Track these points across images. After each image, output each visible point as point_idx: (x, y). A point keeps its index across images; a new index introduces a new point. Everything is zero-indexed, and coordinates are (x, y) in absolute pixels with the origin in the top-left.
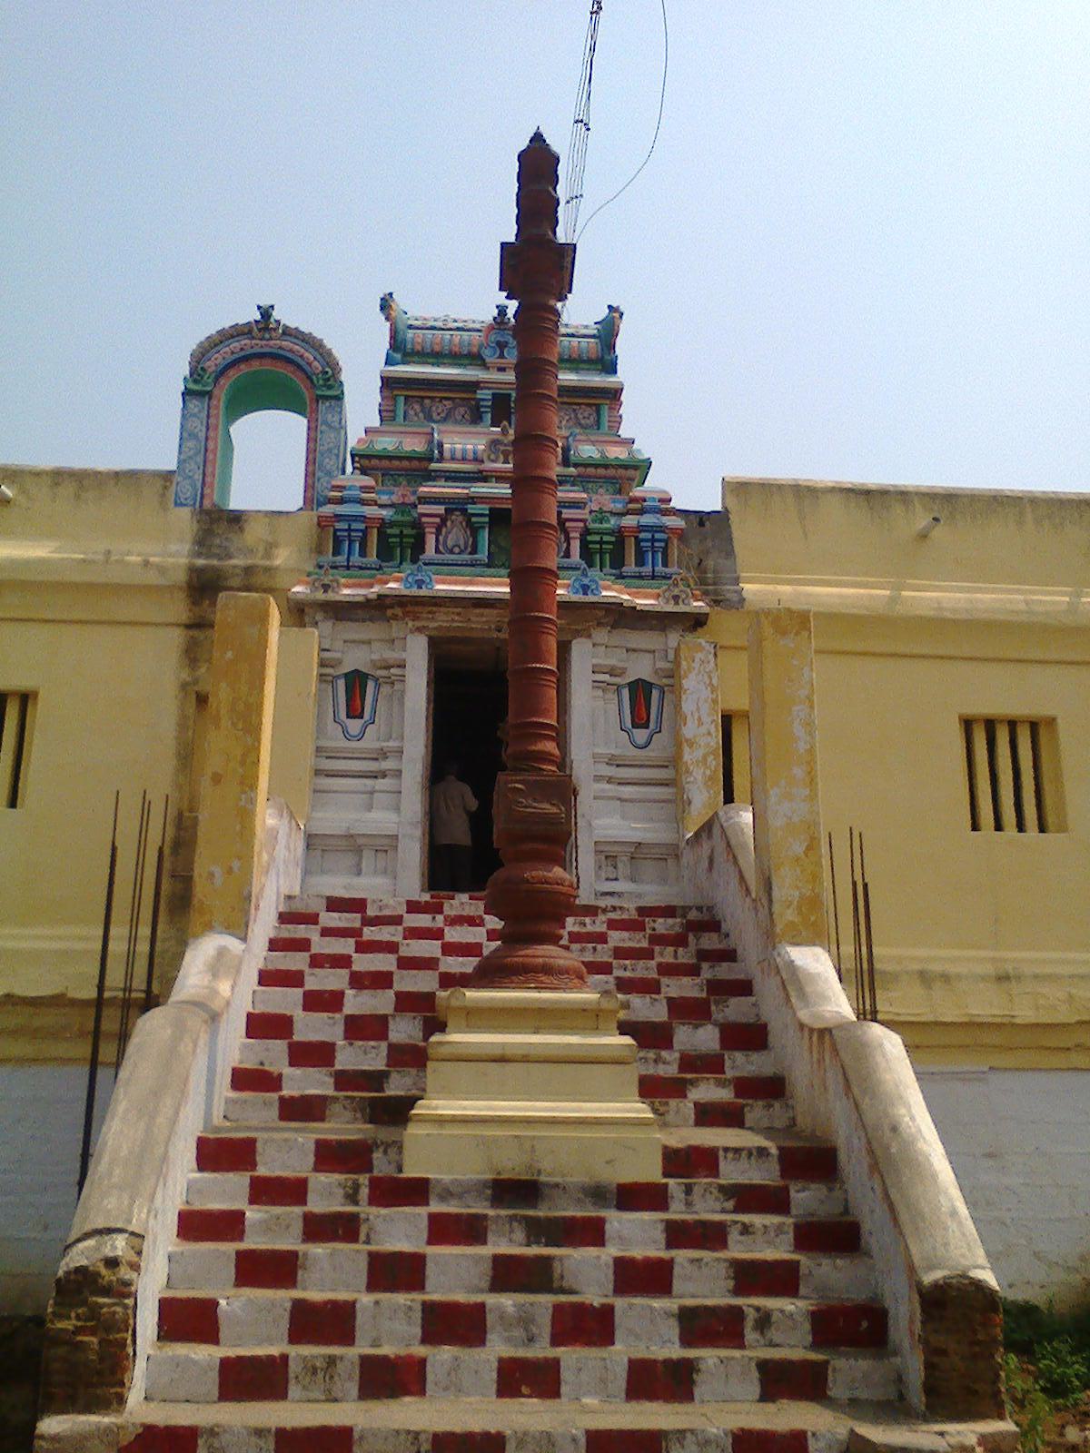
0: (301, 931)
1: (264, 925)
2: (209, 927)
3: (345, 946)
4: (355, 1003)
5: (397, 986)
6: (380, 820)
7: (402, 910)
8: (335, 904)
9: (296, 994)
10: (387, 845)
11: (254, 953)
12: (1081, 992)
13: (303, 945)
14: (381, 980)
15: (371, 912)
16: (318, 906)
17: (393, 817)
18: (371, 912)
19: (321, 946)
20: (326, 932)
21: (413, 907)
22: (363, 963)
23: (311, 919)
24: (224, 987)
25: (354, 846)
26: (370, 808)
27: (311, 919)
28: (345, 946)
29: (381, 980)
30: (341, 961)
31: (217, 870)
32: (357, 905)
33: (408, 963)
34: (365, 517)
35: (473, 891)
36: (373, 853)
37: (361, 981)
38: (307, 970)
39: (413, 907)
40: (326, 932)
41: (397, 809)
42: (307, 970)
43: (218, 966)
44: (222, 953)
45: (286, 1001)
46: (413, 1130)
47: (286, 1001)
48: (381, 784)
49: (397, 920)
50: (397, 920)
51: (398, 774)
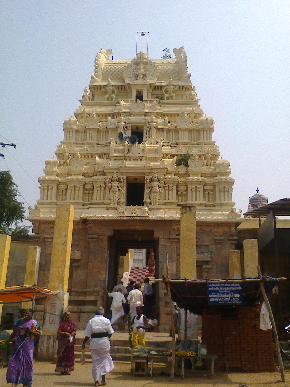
0: (133, 271)
1: (130, 270)
2: (125, 271)
3: (137, 272)
4: (138, 278)
5: (141, 276)
6: (141, 258)
7: (142, 269)
8: (136, 268)
9: (133, 277)
10: (142, 260)
11: (129, 273)
12: (284, 221)
13: (133, 272)
14: (140, 276)
15: (140, 269)
16: (134, 268)
17: (142, 257)
18: (140, 269)
19: (135, 272)
20: (135, 271)
21: (144, 268)
22: (139, 274)
23: (134, 269)
24: (127, 277)
25: (138, 260)
26: (140, 256)
27: (134, 269)
28: (137, 272)
29: (140, 276)
30: (137, 274)
31: (126, 266)
32: (138, 268)
33: (142, 274)
34: (119, 63)
35: (124, 99)
36: (97, 95)
37: (138, 276)
38: (136, 281)
39: (144, 268)
40: (135, 271)
41: (143, 256)
42: (136, 281)
43: (126, 275)
44: (126, 274)
45: (132, 277)
46: (141, 288)
47: (132, 277)
48: (141, 253)
49: (142, 270)
50: (142, 270)
51: (143, 252)
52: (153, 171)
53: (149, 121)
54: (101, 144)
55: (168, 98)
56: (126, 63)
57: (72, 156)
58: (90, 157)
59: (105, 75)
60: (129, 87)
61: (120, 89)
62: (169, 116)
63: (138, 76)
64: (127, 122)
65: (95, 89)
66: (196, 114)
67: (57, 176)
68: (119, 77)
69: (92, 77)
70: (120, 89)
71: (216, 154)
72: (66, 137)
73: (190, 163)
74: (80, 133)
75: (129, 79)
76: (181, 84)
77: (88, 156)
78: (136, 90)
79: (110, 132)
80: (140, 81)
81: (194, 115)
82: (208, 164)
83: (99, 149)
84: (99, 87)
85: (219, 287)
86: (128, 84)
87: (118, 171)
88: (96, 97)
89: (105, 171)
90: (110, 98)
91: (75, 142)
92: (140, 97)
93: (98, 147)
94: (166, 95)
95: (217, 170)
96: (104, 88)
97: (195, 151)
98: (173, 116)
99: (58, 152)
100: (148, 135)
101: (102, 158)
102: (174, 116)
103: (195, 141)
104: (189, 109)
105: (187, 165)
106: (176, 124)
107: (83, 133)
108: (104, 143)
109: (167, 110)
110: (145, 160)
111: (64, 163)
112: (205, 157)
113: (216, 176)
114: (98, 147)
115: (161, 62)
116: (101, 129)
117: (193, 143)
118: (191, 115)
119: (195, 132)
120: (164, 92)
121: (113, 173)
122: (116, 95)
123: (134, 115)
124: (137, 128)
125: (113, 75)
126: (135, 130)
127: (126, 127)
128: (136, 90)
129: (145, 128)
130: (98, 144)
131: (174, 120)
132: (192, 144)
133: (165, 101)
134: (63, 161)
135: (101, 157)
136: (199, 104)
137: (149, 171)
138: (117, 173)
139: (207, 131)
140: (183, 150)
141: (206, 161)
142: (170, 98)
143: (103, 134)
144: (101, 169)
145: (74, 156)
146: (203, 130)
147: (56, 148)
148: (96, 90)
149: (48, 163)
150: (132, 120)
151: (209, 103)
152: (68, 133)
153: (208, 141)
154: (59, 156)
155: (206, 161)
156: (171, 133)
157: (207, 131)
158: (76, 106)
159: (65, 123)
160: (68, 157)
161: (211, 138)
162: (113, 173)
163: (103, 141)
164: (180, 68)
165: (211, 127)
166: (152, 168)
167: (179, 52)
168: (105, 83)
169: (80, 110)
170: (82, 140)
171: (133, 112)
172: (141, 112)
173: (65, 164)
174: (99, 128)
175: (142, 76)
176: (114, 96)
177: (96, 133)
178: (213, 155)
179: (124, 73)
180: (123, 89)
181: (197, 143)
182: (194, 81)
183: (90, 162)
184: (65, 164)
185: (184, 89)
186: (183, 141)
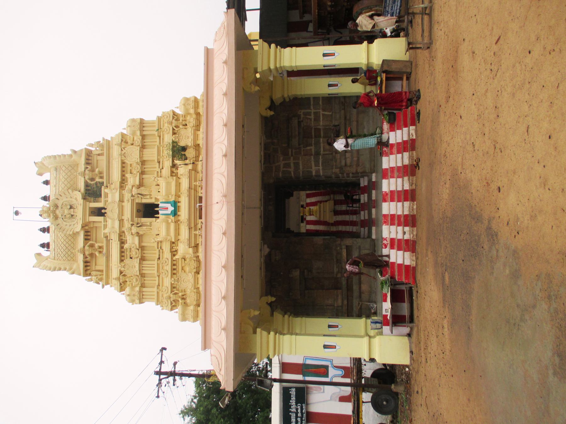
52: (193, 187)
53: (130, 195)
54: (159, 255)
55: (102, 178)
56: (54, 232)
57: (175, 289)
58: (175, 267)
59: (69, 258)
60: (86, 225)
61: (89, 237)
62: (124, 173)
63: (72, 216)
64: (132, 223)
65: (87, 270)
66: (122, 140)
67: (199, 305)
68: (72, 240)
69: (73, 273)
70: (89, 237)
71: (172, 114)
72: (151, 299)
73: (182, 144)
74: (145, 282)
75: (76, 225)
76: (83, 160)
77: (174, 269)
78: (89, 216)
79: (143, 244)
80: (79, 212)
81: (123, 143)
82: (184, 123)
83: (165, 256)
84: (86, 264)
85: (297, 413)
86: (83, 227)
87: (193, 229)
88: (98, 268)
89: (193, 245)
90: (100, 250)
91: (156, 287)
92: (99, 212)
93: (162, 286)
94: (98, 180)
95: (192, 111)
96: (87, 258)
97: (168, 138)
98: (124, 165)
99: (170, 307)
100: (148, 197)
101: (177, 253)
102: (123, 171)
103: (155, 166)
104: (116, 151)
105: (184, 149)
106: (135, 164)
107: (145, 278)
108: (157, 252)
109: (116, 176)
110: (179, 197)
111: (183, 299)
112: (175, 127)
113: (199, 145)
114: (162, 286)
115: (54, 188)
116: (140, 256)
117: (158, 143)
118: (123, 146)
119: (145, 167)
120: (92, 183)
121: (195, 235)
122: (96, 242)
123: (122, 215)
124: (138, 211)
125: (69, 248)
126: (142, 213)
127: (138, 223)
128: (89, 216)
129: (138, 200)
130: (159, 258)
131: (129, 166)
132: (160, 143)
133: (105, 180)
134: (180, 300)
135: (175, 253)
136: (110, 139)
137: (193, 191)
138: (195, 230)
139: (143, 127)
140: (167, 153)
141: (181, 127)
142: (101, 175)
143: (147, 254)
144: (191, 250)
145: (174, 288)
146: (141, 130)
147: (164, 310)
148: (89, 268)
149: (184, 318)
150: (129, 216)
151: (108, 125)
152: (144, 297)
153: (156, 125)
154: (174, 306)
155: (181, 127)
156: (145, 170)
157: (143, 127)
158: (111, 292)
159: (133, 301)
160: (176, 294)
161: (153, 122)
162: (195, 235)
163: (155, 254)
164: (61, 164)
165: (139, 121)
166: (190, 188)
167: (41, 168)
168: (81, 257)
169: (115, 284)
170: (153, 279)
171: (119, 216)
172: (119, 205)
173: (184, 297)
174: (138, 259)
175: (72, 210)
176: (97, 245)
177: (144, 262)
178: (173, 118)
179: (68, 233)
180: (89, 234)
181: (158, 138)
182: (81, 145)
183: (182, 267)
184: (184, 297)
185: (90, 158)
186: (156, 155)
